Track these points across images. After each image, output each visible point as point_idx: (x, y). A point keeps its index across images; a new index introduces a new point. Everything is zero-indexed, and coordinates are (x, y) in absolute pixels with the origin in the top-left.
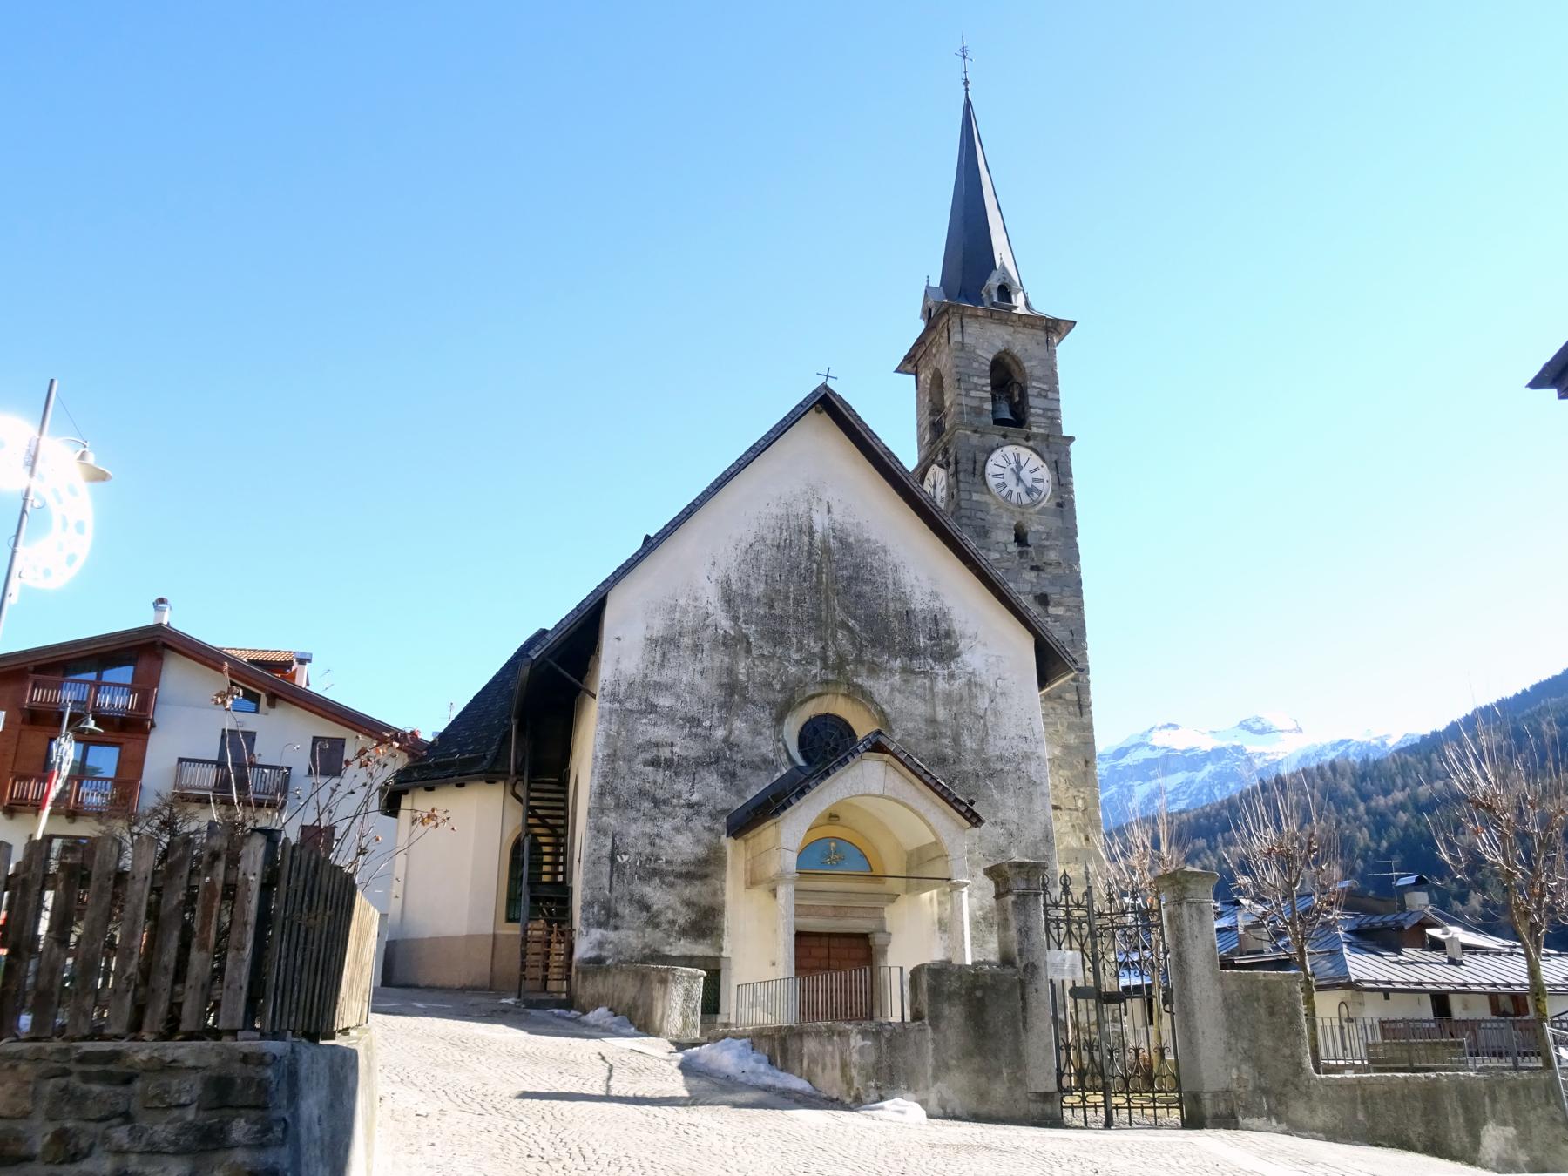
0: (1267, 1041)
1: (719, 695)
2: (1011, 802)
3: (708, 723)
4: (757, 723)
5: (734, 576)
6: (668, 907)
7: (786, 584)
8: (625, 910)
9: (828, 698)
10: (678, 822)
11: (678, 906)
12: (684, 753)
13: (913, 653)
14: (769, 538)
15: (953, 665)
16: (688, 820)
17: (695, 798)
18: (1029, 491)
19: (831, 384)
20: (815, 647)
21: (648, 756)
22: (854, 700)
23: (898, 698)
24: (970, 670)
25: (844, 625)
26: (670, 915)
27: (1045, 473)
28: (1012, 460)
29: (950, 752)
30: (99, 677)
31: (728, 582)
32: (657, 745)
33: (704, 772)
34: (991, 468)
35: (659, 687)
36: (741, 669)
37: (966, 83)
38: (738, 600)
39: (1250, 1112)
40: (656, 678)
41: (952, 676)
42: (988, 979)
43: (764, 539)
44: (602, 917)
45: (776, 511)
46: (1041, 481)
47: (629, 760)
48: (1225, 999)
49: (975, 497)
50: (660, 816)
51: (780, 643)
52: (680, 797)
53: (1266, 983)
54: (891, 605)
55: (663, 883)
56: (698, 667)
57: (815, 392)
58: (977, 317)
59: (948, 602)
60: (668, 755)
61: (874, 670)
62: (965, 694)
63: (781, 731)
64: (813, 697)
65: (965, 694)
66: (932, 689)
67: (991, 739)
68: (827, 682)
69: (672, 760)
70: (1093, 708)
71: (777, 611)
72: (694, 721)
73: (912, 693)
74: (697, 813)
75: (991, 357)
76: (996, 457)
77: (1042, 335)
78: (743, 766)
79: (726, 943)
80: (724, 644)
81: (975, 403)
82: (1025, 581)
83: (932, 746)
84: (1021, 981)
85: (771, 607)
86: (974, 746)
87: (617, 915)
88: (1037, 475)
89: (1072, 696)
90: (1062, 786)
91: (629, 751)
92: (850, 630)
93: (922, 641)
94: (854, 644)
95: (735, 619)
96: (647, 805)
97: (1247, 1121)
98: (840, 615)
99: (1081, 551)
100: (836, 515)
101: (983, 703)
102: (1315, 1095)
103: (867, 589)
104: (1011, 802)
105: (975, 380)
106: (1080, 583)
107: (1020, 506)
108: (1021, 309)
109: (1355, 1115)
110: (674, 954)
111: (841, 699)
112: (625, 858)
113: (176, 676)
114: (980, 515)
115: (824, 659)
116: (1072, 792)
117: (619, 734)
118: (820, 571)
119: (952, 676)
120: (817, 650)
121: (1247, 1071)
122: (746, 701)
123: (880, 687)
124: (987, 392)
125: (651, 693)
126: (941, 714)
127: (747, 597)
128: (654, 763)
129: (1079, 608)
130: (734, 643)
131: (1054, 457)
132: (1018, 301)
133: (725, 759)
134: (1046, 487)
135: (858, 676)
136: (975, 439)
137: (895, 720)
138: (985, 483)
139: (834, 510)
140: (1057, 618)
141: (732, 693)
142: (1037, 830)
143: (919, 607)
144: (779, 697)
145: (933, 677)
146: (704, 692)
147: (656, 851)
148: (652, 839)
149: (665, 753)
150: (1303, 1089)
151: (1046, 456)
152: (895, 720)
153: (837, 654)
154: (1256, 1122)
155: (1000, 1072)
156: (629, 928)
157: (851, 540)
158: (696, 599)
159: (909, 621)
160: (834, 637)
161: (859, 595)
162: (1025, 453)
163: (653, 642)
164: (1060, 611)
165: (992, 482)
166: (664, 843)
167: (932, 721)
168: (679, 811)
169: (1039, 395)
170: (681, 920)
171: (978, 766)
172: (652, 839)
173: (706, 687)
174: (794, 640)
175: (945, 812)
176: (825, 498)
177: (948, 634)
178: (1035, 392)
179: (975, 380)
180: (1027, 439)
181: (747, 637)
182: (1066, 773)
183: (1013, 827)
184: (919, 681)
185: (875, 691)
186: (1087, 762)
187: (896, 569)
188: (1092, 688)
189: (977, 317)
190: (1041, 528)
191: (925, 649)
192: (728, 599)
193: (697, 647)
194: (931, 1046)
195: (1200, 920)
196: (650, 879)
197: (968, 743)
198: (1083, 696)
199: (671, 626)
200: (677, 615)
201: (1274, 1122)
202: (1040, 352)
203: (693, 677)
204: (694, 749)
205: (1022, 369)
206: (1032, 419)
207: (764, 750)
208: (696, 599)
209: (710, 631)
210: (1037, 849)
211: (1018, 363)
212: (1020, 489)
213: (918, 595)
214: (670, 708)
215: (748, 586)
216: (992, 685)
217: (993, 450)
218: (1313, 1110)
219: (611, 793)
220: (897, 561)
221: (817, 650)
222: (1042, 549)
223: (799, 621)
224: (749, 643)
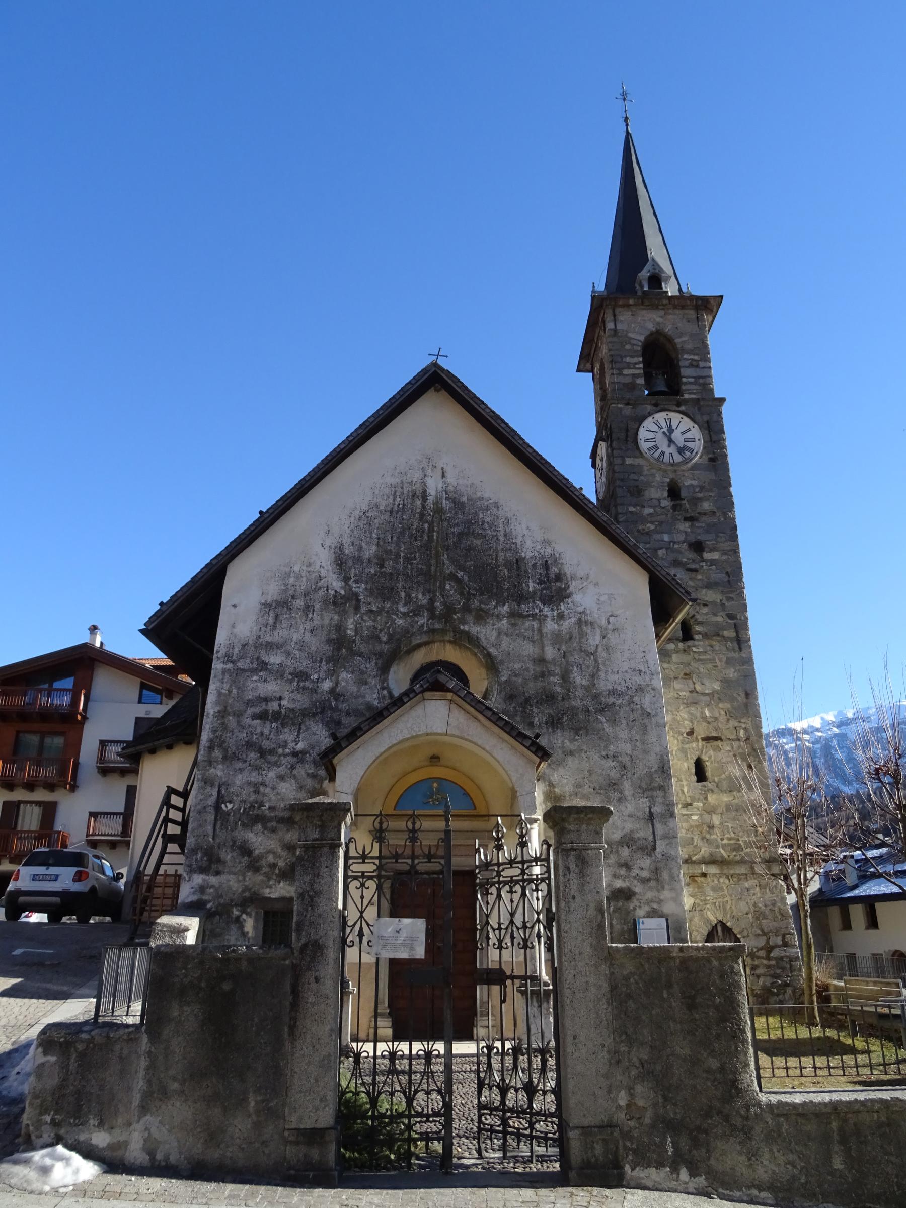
0: (682, 1048)
1: (327, 649)
2: (623, 735)
3: (316, 677)
4: (363, 673)
5: (346, 541)
6: (269, 852)
7: (398, 545)
8: (227, 856)
9: (436, 645)
10: (282, 770)
12: (292, 706)
13: (522, 598)
14: (383, 505)
15: (563, 607)
16: (293, 767)
17: (300, 746)
18: (681, 451)
19: (442, 362)
20: (423, 600)
21: (257, 710)
22: (461, 646)
23: (505, 641)
24: (580, 609)
25: (453, 577)
26: (271, 858)
27: (696, 433)
28: (664, 425)
29: (558, 689)
30: (51, 685)
31: (341, 547)
32: (266, 700)
33: (310, 723)
34: (643, 434)
35: (271, 646)
36: (350, 624)
37: (626, 119)
38: (350, 563)
39: (643, 1159)
40: (268, 638)
41: (561, 616)
42: (244, 965)
43: (377, 506)
44: (205, 864)
45: (390, 480)
46: (693, 440)
47: (239, 715)
48: (613, 988)
49: (629, 461)
50: (265, 766)
51: (388, 599)
52: (285, 747)
53: (684, 961)
54: (502, 555)
55: (265, 828)
56: (308, 626)
57: (424, 371)
58: (629, 306)
59: (559, 548)
60: (276, 708)
61: (481, 616)
62: (575, 632)
63: (386, 680)
64: (419, 646)
65: (575, 632)
66: (540, 630)
67: (602, 674)
68: (432, 631)
69: (279, 713)
70: (752, 643)
71: (388, 569)
72: (302, 676)
74: (301, 761)
75: (642, 338)
76: (648, 423)
77: (692, 313)
78: (348, 714)
80: (334, 603)
81: (628, 380)
82: (679, 532)
83: (539, 684)
84: (294, 967)
85: (382, 566)
86: (585, 682)
87: (219, 861)
88: (689, 435)
89: (729, 633)
90: (723, 718)
91: (238, 706)
92: (459, 581)
93: (532, 586)
94: (461, 594)
95: (346, 579)
96: (253, 755)
97: (640, 1173)
98: (449, 569)
99: (735, 500)
100: (450, 479)
101: (594, 640)
102: (758, 1129)
103: (478, 542)
104: (623, 735)
105: (628, 360)
106: (735, 528)
107: (673, 464)
108: (671, 289)
109: (828, 1159)
110: (273, 896)
111: (449, 647)
112: (230, 806)
113: (104, 682)
114: (632, 476)
115: (431, 608)
116: (733, 723)
117: (230, 691)
118: (431, 530)
119: (561, 616)
120: (425, 602)
121: (644, 1095)
122: (353, 653)
123: (487, 633)
124: (639, 369)
125: (263, 652)
126: (550, 653)
127: (358, 560)
128: (263, 716)
129: (735, 551)
130: (344, 602)
131: (706, 418)
132: (671, 289)
133: (331, 708)
134: (698, 446)
135: (464, 623)
136: (628, 411)
137: (502, 662)
138: (638, 448)
139: (448, 475)
140: (712, 562)
141: (340, 648)
142: (652, 761)
143: (529, 554)
144: (385, 648)
145: (541, 619)
146: (313, 648)
147: (260, 798)
148: (256, 788)
149: (274, 706)
150: (738, 1122)
151: (698, 417)
152: (502, 662)
153: (444, 604)
154: (653, 1174)
155: (245, 1100)
156: (230, 873)
157: (464, 499)
158: (310, 565)
159: (519, 568)
160: (442, 588)
161: (469, 549)
162: (675, 418)
163: (267, 606)
164: (715, 556)
165: (644, 446)
166: (268, 790)
168: (284, 760)
169: (691, 366)
170: (281, 864)
171: (588, 701)
172: (256, 788)
173: (315, 643)
174: (403, 594)
175: (513, 748)
176: (440, 465)
177: (559, 578)
178: (687, 363)
179: (628, 360)
180: (679, 405)
181: (356, 595)
182: (727, 705)
184: (527, 624)
185: (482, 636)
186: (747, 695)
187: (508, 522)
188: (750, 624)
189: (629, 306)
190: (695, 483)
191: (534, 592)
192: (341, 562)
193: (308, 609)
194: (143, 1063)
195: (582, 874)
196: (253, 825)
197: (578, 680)
198: (742, 632)
199: (285, 591)
200: (292, 581)
201: (684, 1174)
202: (692, 328)
203: (303, 634)
204: (302, 701)
205: (674, 345)
206: (684, 387)
207: (368, 698)
208: (310, 565)
209: (321, 593)
210: (652, 779)
211: (670, 340)
212: (673, 449)
213: (529, 544)
214: (281, 665)
215: (360, 549)
216: (604, 622)
217: (644, 418)
218: (753, 1155)
219: (220, 746)
220: (509, 515)
221: (425, 602)
222: (695, 501)
223: (408, 577)
224: (358, 601)
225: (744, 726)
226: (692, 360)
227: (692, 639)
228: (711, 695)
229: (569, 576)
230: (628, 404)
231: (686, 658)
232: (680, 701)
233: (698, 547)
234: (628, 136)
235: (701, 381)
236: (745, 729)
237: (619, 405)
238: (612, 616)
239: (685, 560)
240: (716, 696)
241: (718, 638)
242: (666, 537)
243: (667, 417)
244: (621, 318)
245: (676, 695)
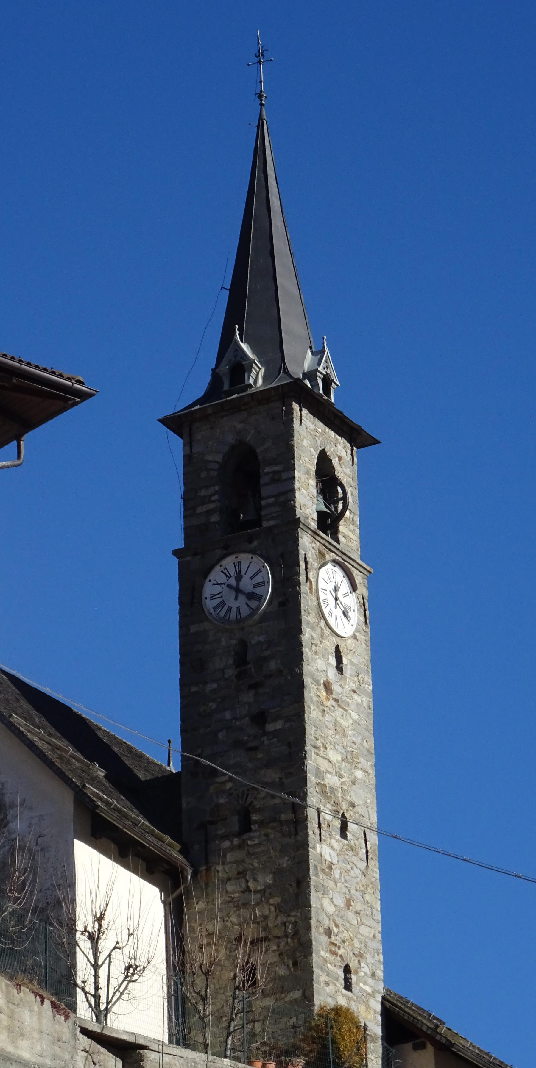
140: (275, 734)
164: (278, 725)
165: (209, 604)
179: (203, 493)
180: (250, 541)
190: (262, 638)
225: (293, 920)
226: (274, 472)
227: (250, 830)
228: (262, 892)
229: (7, 806)
230: (195, 554)
231: (239, 855)
232: (231, 905)
233: (260, 719)
234: (261, 120)
235: (282, 499)
236: (295, 924)
237: (188, 558)
238: (40, 837)
239: (246, 738)
240: (268, 891)
241: (275, 824)
242: (228, 715)
243: (222, 568)
244: (198, 436)
245: (228, 899)
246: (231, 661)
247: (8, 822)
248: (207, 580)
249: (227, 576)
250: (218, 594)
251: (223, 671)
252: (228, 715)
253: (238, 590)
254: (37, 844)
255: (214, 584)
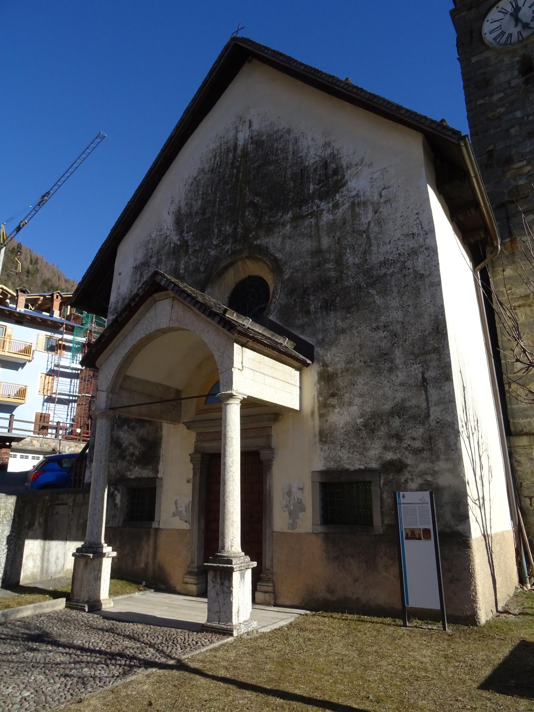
11: (136, 443)
15: (338, 197)
26: (131, 449)
43: (203, 170)
61: (270, 229)
66: (317, 225)
67: (374, 248)
73: (303, 235)
79: (161, 468)
86: (357, 261)
110: (132, 477)
119: (336, 206)
126: (326, 242)
137: (285, 263)
152: (285, 263)
167: (318, 252)
174: (216, 230)
183: (397, 328)
184: (306, 222)
197: (351, 260)
199: (146, 254)
216: (376, 197)
229: (345, 167)
238: (384, 189)
246: (516, 73)
247: (346, 182)
248: (486, 20)
249: (504, 13)
250: (497, 28)
251: (509, 82)
252: (518, 114)
253: (517, 20)
254: (381, 196)
255: (491, 23)
